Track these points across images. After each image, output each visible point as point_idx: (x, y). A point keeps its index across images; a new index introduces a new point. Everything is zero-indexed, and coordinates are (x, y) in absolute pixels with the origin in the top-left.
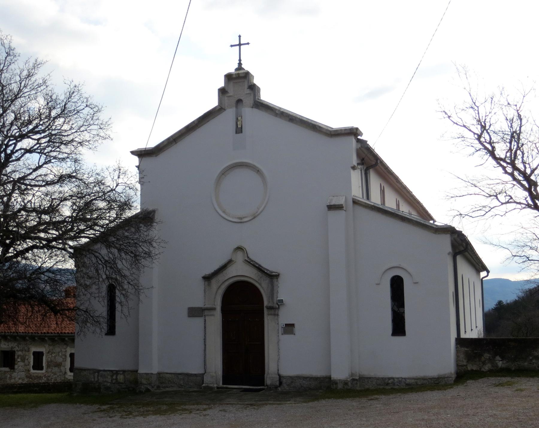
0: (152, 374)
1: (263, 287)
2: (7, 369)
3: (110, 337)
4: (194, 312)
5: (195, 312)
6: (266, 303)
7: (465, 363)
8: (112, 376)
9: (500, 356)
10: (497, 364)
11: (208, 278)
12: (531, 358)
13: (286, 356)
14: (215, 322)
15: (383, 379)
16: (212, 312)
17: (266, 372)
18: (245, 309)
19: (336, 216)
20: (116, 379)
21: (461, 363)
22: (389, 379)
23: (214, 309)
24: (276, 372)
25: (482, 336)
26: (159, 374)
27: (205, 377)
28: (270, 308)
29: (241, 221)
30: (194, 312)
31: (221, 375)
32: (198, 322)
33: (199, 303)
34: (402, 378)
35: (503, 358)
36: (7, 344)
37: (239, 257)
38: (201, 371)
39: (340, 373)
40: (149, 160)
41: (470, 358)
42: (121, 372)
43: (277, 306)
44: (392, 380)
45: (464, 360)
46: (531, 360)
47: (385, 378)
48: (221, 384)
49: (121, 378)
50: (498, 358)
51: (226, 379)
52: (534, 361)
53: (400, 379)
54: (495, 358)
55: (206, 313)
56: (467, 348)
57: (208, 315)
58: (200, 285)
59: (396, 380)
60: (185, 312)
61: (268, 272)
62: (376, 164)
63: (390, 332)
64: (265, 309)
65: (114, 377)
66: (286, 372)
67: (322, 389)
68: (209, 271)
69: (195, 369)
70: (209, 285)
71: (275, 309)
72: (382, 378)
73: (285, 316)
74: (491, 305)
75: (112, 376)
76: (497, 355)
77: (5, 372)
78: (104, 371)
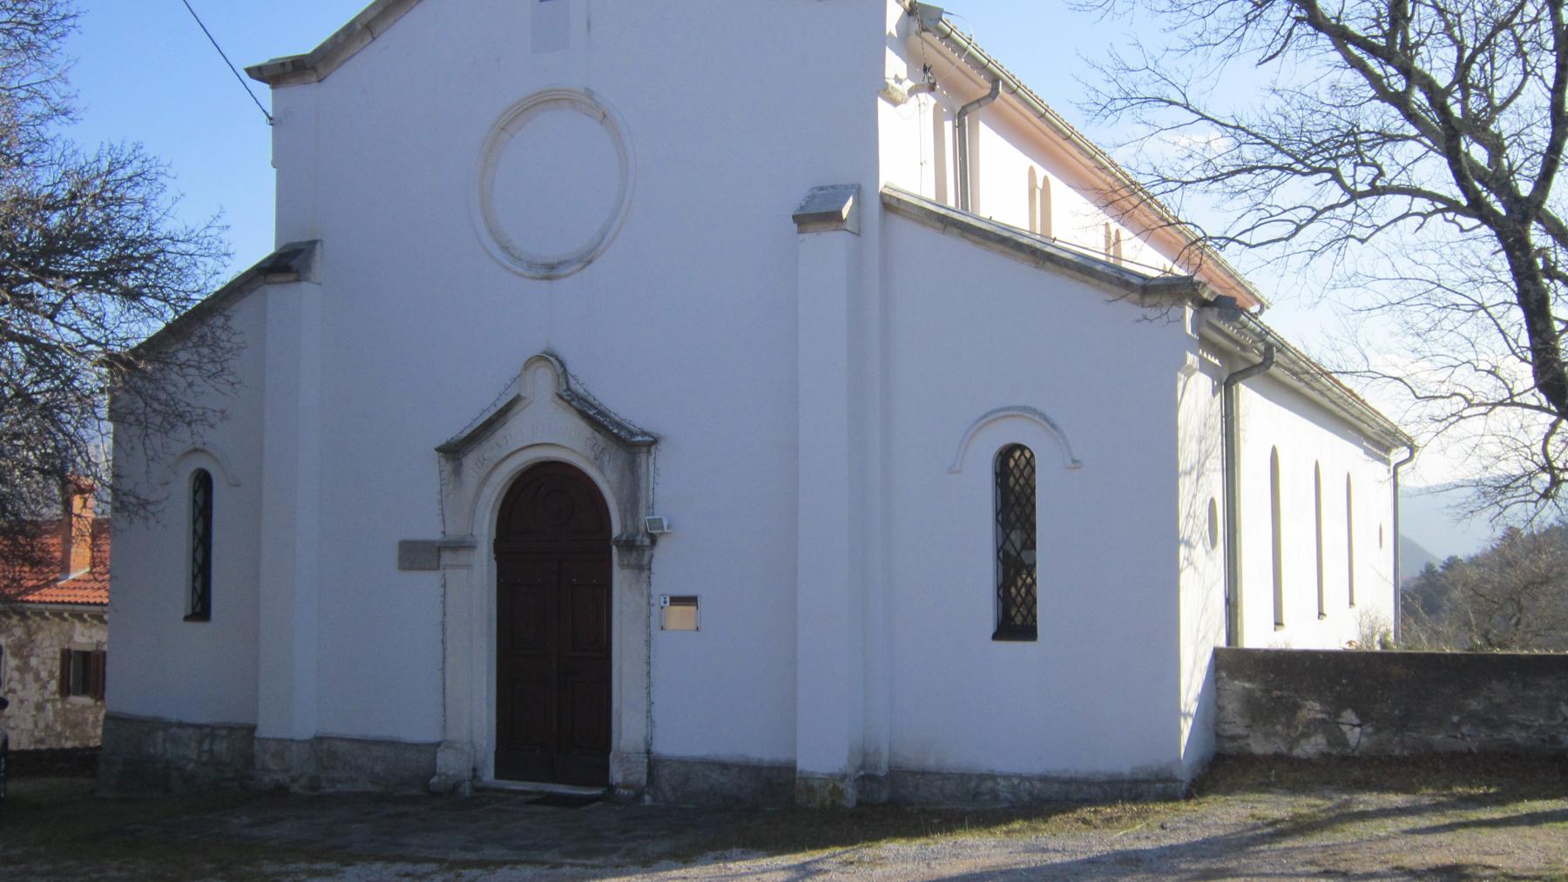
0: (292, 740)
1: (606, 481)
2: (87, 700)
3: (199, 627)
4: (418, 555)
5: (419, 555)
6: (616, 530)
7: (1241, 731)
8: (200, 742)
9: (1355, 710)
10: (1344, 734)
11: (454, 451)
12: (1456, 719)
13: (675, 691)
14: (475, 583)
15: (964, 777)
16: (463, 557)
17: (614, 747)
18: (559, 551)
19: (828, 245)
20: (211, 751)
21: (1230, 730)
22: (982, 777)
23: (471, 547)
24: (642, 748)
25: (628, 730)
26: (319, 739)
27: (440, 755)
28: (629, 545)
29: (550, 271)
30: (418, 555)
31: (493, 748)
32: (426, 582)
33: (429, 530)
34: (1021, 777)
35: (1364, 718)
36: (87, 633)
37: (543, 383)
38: (434, 737)
39: (822, 753)
40: (301, 94)
41: (1260, 712)
42: (224, 732)
43: (647, 541)
44: (990, 784)
45: (1238, 720)
46: (1457, 726)
47: (970, 777)
48: (488, 775)
49: (221, 747)
50: (1349, 716)
51: (507, 761)
52: (1465, 729)
53: (1016, 782)
54: (1339, 716)
55: (447, 557)
56: (1250, 680)
57: (452, 566)
58: (432, 468)
59: (1002, 782)
60: (393, 556)
61: (623, 434)
62: (1268, 358)
63: (990, 626)
64: (615, 550)
65: (206, 746)
66: (670, 745)
67: (770, 805)
68: (456, 426)
69: (419, 730)
70: (457, 472)
71: (641, 547)
72: (962, 776)
73: (671, 567)
74: (1414, 570)
75: (200, 742)
76: (1345, 708)
77: (84, 708)
78: (181, 725)
